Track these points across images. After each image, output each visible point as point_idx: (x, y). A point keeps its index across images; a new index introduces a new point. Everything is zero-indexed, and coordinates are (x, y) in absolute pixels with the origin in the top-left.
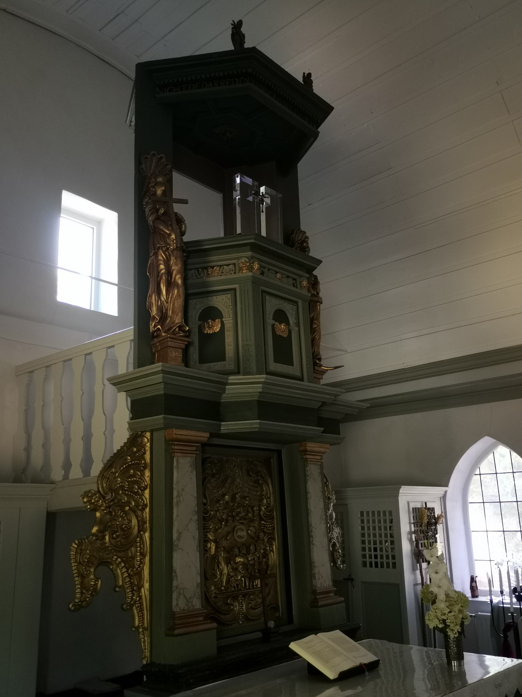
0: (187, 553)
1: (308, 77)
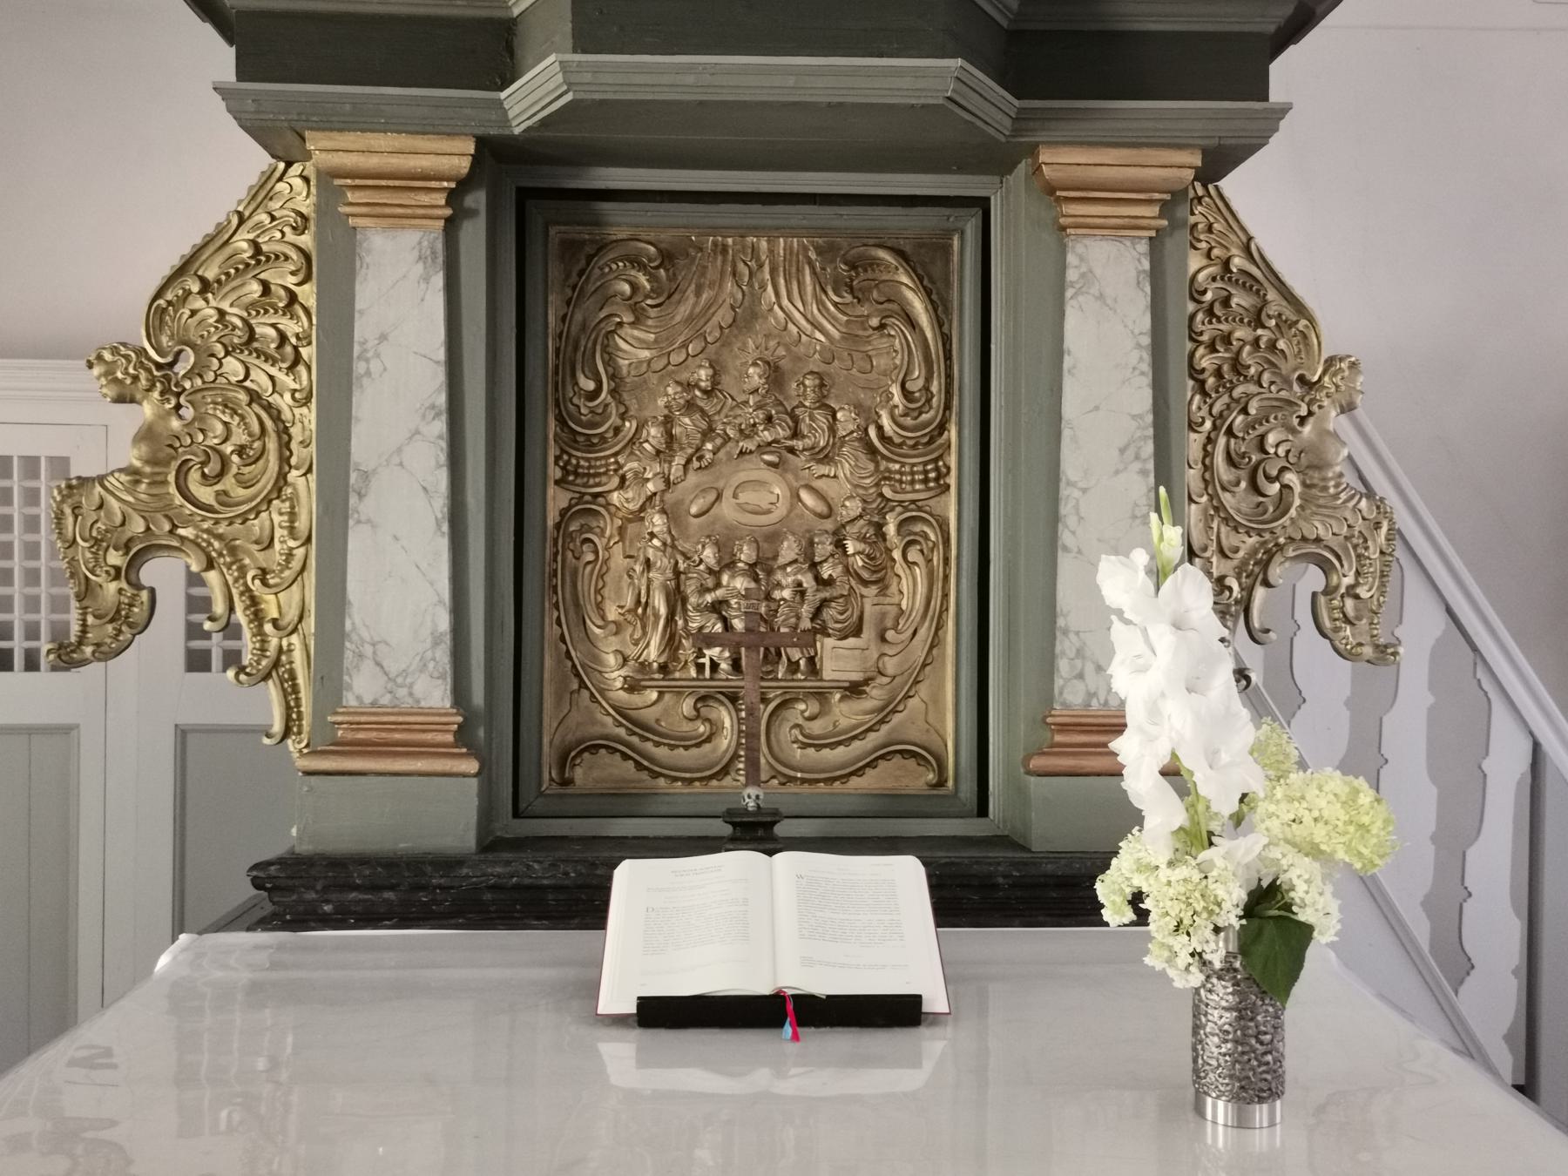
0: (396, 538)
1: (1284, 110)
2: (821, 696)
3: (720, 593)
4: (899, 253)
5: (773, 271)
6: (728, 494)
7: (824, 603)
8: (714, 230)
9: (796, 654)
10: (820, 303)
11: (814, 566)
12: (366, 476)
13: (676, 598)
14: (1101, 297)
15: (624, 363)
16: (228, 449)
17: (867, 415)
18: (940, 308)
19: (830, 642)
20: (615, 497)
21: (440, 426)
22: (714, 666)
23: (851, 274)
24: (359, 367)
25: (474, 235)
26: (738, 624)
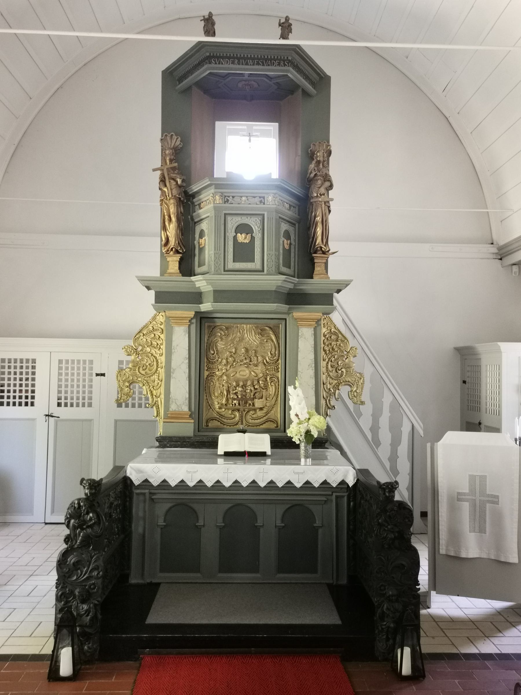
2: (255, 410)
3: (236, 391)
4: (270, 328)
5: (247, 331)
6: (238, 372)
7: (256, 393)
8: (236, 324)
9: (250, 402)
10: (255, 337)
11: (254, 386)
12: (174, 370)
13: (228, 392)
14: (305, 338)
15: (219, 348)
16: (147, 364)
17: (264, 357)
18: (277, 338)
19: (256, 400)
20: (217, 373)
21: (187, 361)
22: (235, 404)
23: (262, 332)
24: (173, 351)
25: (193, 327)
26: (240, 397)
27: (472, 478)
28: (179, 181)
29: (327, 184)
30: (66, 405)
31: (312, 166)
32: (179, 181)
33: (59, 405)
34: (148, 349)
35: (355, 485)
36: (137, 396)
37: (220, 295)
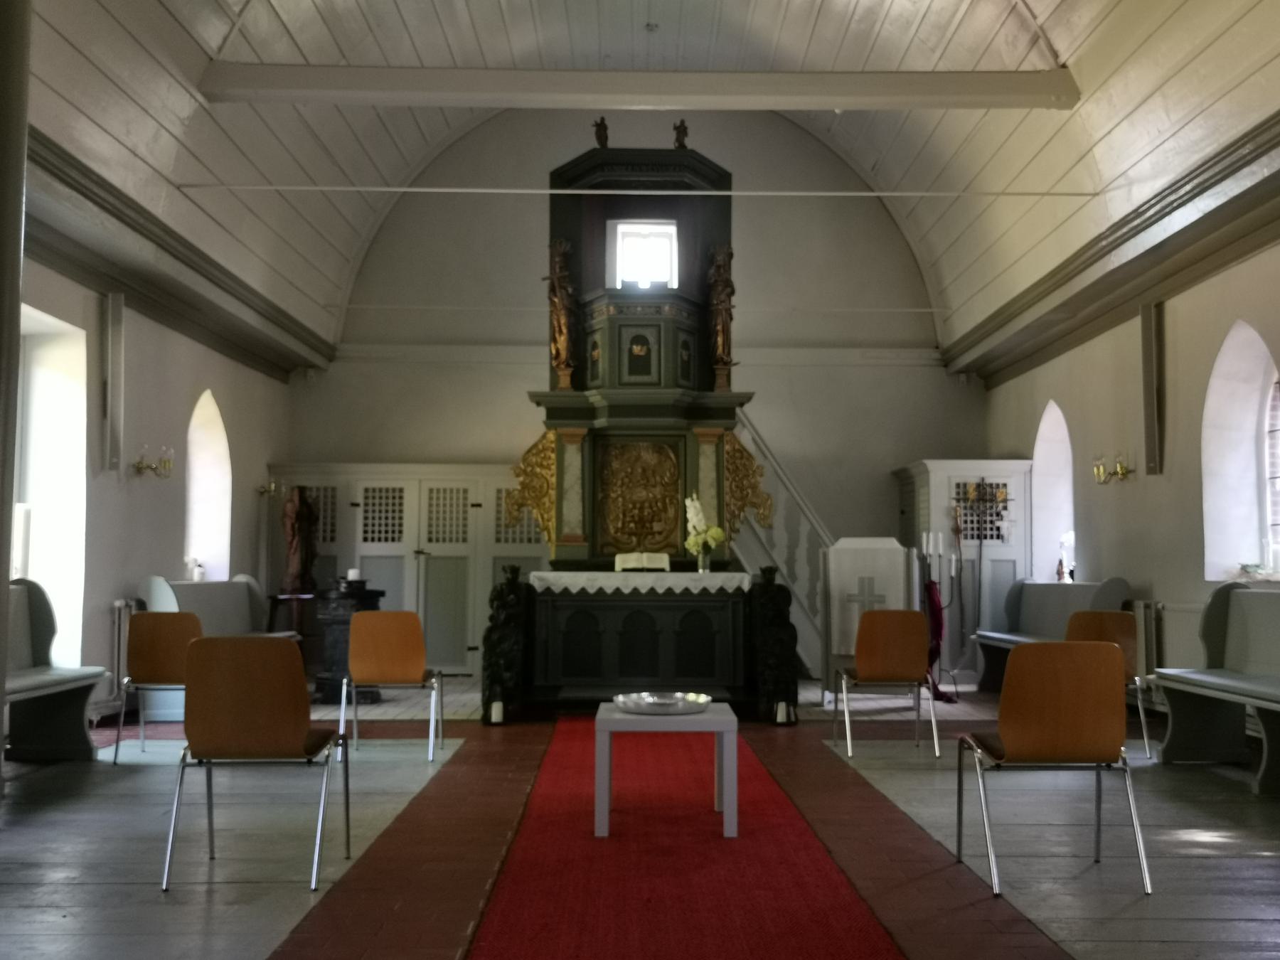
13: (624, 515)
23: (659, 450)
25: (587, 446)
27: (862, 580)
28: (570, 290)
29: (729, 290)
30: (437, 540)
31: (712, 271)
32: (570, 290)
33: (430, 540)
34: (538, 470)
35: (751, 591)
36: (525, 522)
37: (615, 410)
